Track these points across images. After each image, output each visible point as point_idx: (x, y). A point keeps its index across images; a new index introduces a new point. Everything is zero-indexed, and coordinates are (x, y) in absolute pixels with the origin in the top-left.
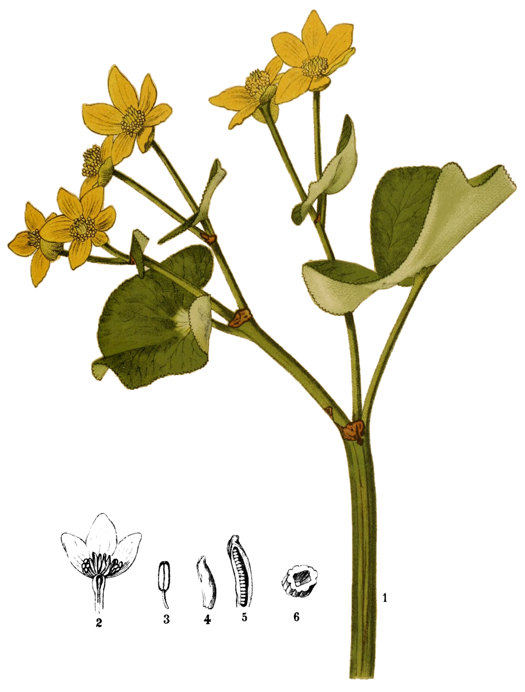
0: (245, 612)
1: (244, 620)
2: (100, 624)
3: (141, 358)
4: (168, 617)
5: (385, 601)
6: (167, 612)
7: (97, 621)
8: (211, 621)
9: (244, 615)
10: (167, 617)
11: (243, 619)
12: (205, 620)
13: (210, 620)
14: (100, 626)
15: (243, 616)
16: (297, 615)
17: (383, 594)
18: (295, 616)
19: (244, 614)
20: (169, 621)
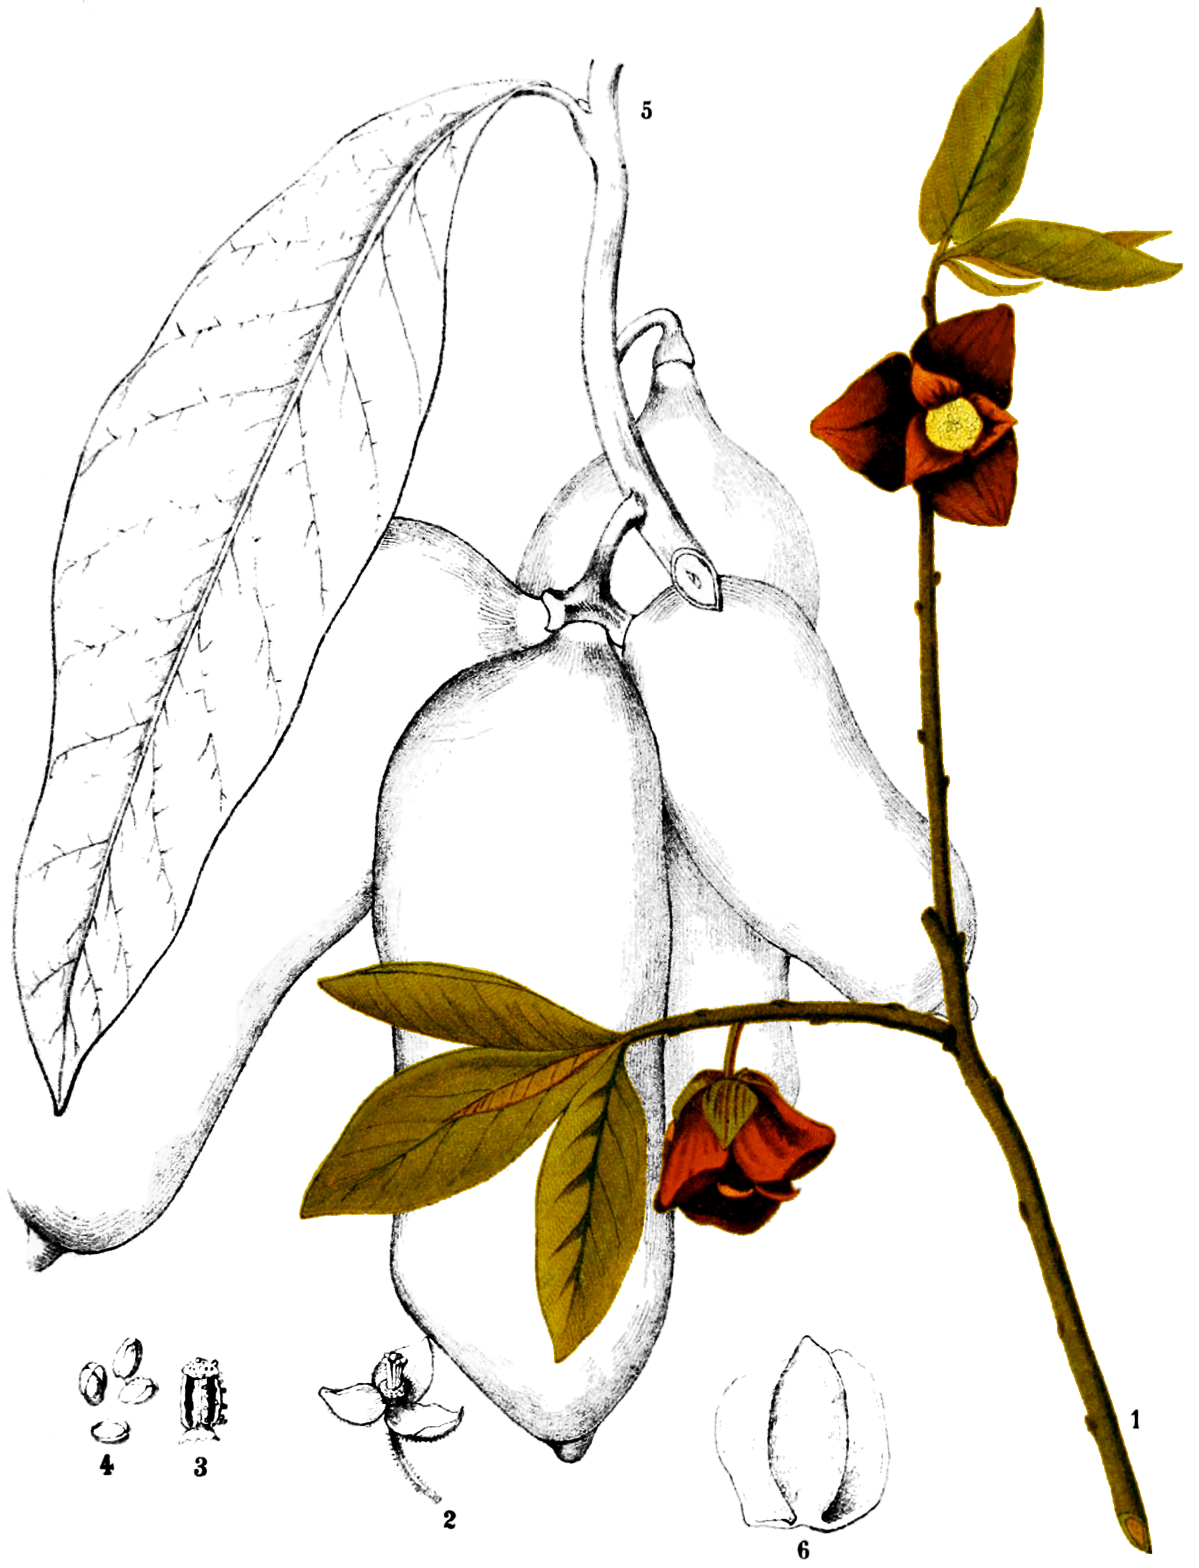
0: (647, 100)
1: (646, 115)
2: (451, 1523)
3: (441, 1146)
4: (205, 1461)
5: (1136, 1426)
6: (255, 572)
7: (446, 1515)
8: (115, 1467)
9: (646, 106)
10: (201, 1461)
11: (643, 115)
12: (102, 1467)
13: (112, 1465)
14: (452, 1527)
15: (645, 108)
16: (804, 1546)
17: (1132, 1412)
18: (800, 1549)
19: (646, 103)
20: (204, 1472)
